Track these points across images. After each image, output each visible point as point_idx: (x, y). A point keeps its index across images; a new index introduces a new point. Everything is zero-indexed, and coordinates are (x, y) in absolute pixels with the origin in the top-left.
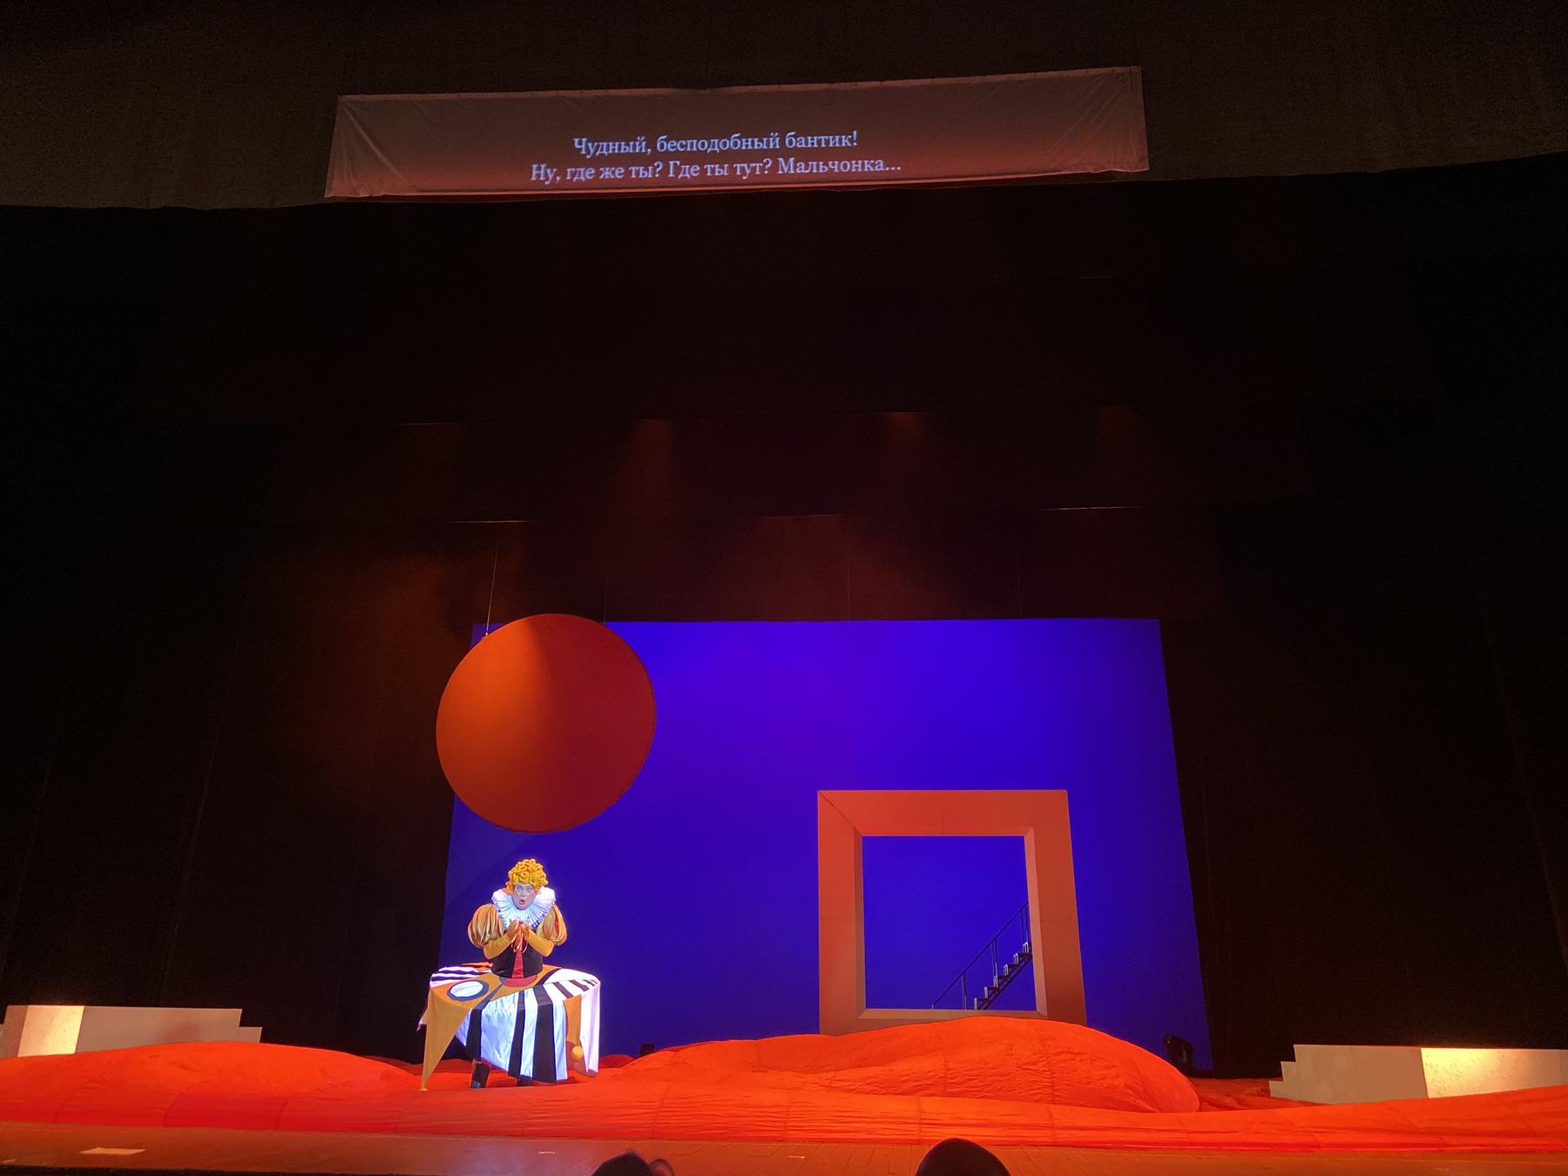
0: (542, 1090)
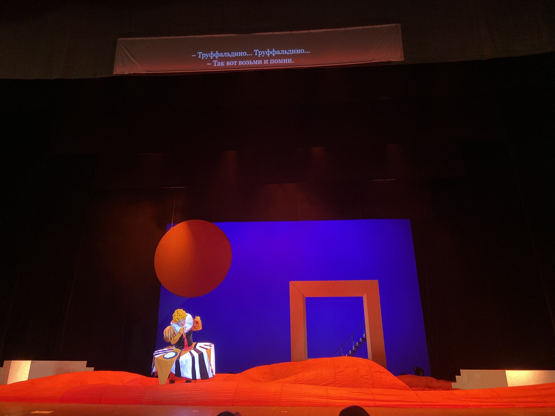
0: (205, 383)
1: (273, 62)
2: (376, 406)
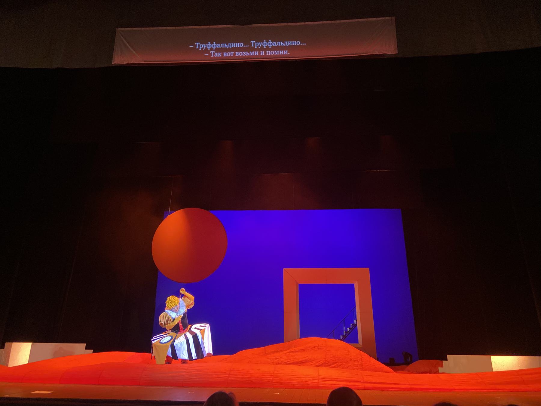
1: (269, 53)
2: (365, 389)
